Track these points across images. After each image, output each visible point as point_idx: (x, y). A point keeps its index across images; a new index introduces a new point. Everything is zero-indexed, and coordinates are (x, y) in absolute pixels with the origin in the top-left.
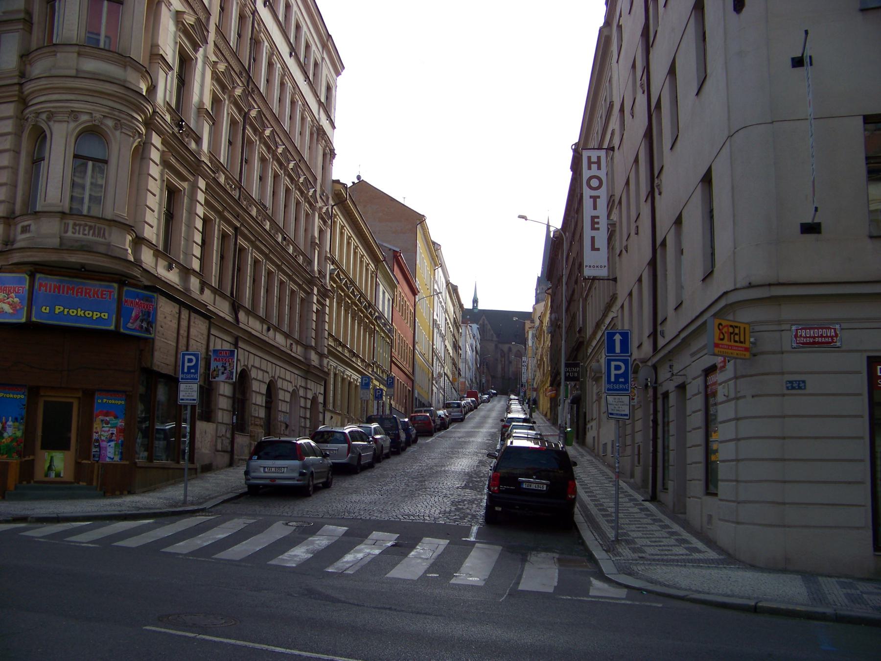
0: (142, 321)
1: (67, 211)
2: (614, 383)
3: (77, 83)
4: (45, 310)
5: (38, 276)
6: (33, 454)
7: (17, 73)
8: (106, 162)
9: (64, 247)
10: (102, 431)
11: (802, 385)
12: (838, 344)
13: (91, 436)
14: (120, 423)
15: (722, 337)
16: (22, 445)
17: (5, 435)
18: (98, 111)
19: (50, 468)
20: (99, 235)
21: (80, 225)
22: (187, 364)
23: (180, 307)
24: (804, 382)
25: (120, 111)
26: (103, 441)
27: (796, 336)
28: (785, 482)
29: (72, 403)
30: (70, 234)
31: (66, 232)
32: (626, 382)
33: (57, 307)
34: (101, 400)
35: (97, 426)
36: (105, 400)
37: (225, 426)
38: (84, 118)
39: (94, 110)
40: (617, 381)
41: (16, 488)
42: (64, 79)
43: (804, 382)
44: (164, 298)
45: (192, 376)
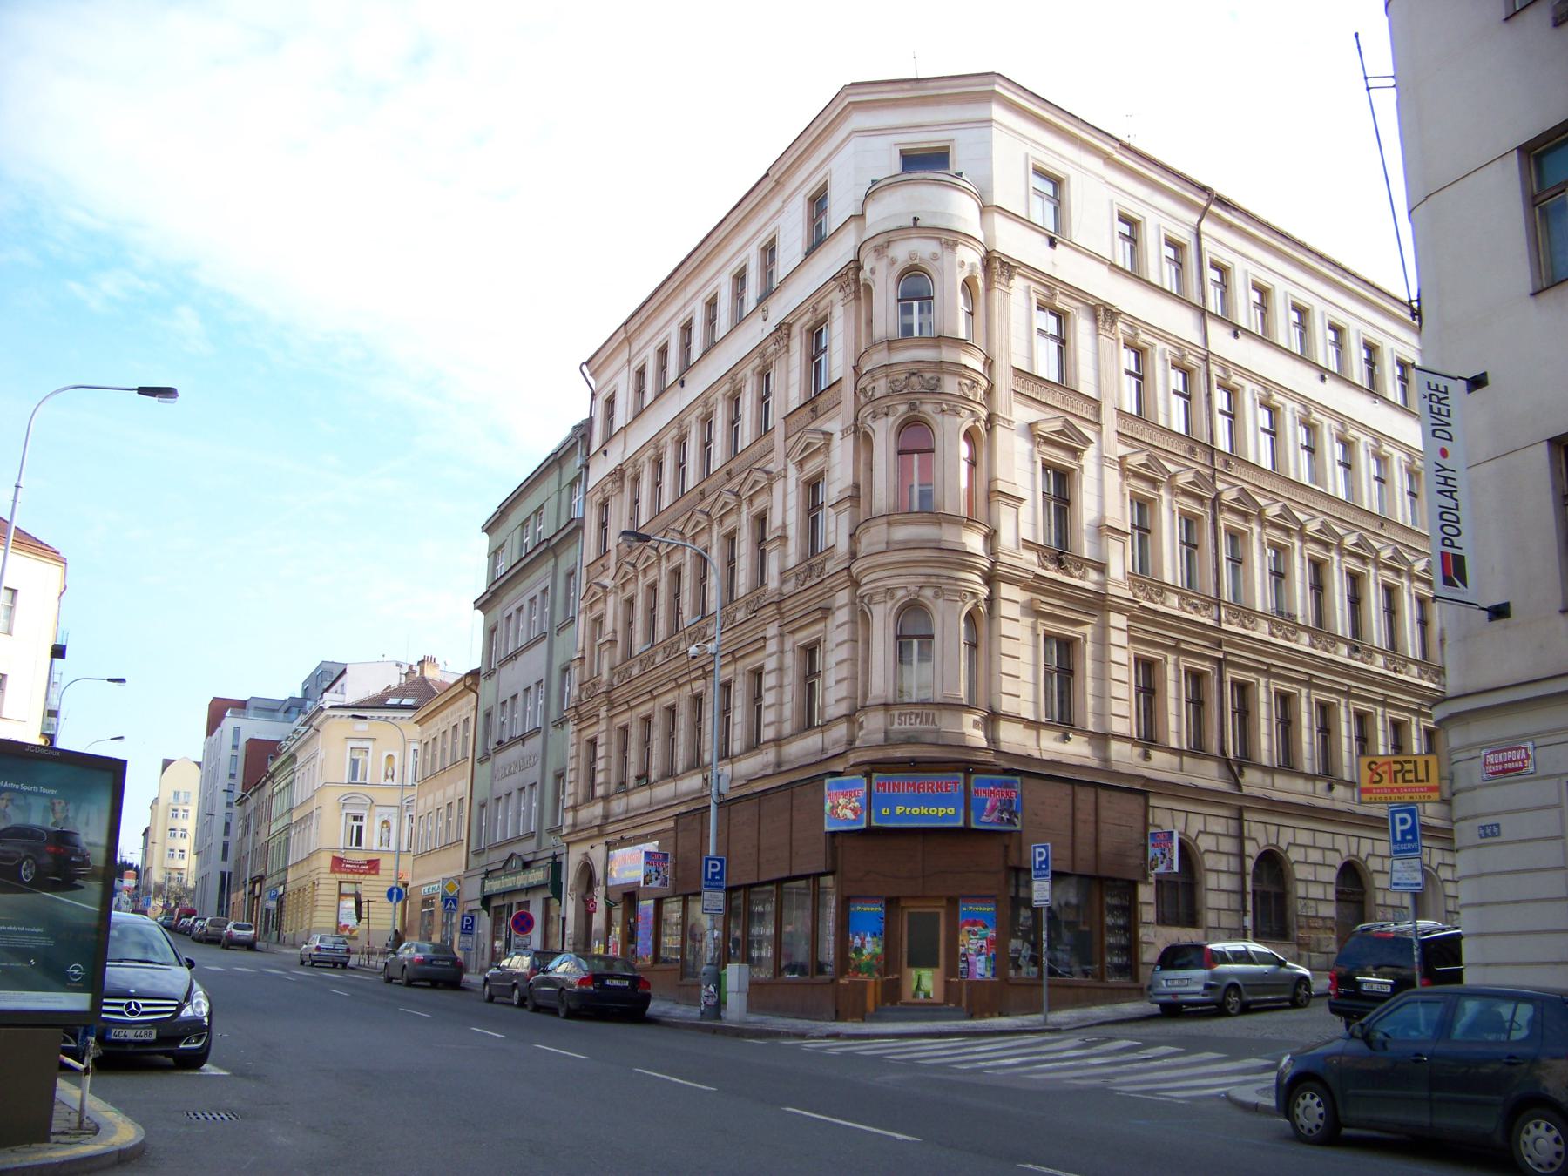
0: (1001, 812)
1: (891, 701)
2: (1401, 842)
3: (888, 558)
5: (875, 775)
6: (900, 972)
7: (848, 556)
8: (932, 637)
9: (889, 741)
10: (969, 943)
11: (1495, 830)
12: (1531, 769)
13: (958, 950)
14: (991, 933)
15: (1377, 778)
16: (883, 962)
17: (865, 952)
18: (913, 583)
19: (918, 988)
20: (927, 722)
21: (906, 714)
22: (1399, 828)
23: (1073, 788)
24: (1498, 826)
25: (938, 576)
26: (971, 955)
27: (1485, 765)
28: (1487, 965)
29: (938, 914)
30: (896, 726)
31: (892, 724)
32: (1415, 839)
33: (898, 807)
34: (967, 908)
35: (963, 938)
36: (970, 908)
37: (1227, 931)
38: (900, 593)
39: (908, 583)
40: (1404, 840)
41: (876, 1010)
42: (875, 556)
43: (1498, 826)
45: (717, 883)
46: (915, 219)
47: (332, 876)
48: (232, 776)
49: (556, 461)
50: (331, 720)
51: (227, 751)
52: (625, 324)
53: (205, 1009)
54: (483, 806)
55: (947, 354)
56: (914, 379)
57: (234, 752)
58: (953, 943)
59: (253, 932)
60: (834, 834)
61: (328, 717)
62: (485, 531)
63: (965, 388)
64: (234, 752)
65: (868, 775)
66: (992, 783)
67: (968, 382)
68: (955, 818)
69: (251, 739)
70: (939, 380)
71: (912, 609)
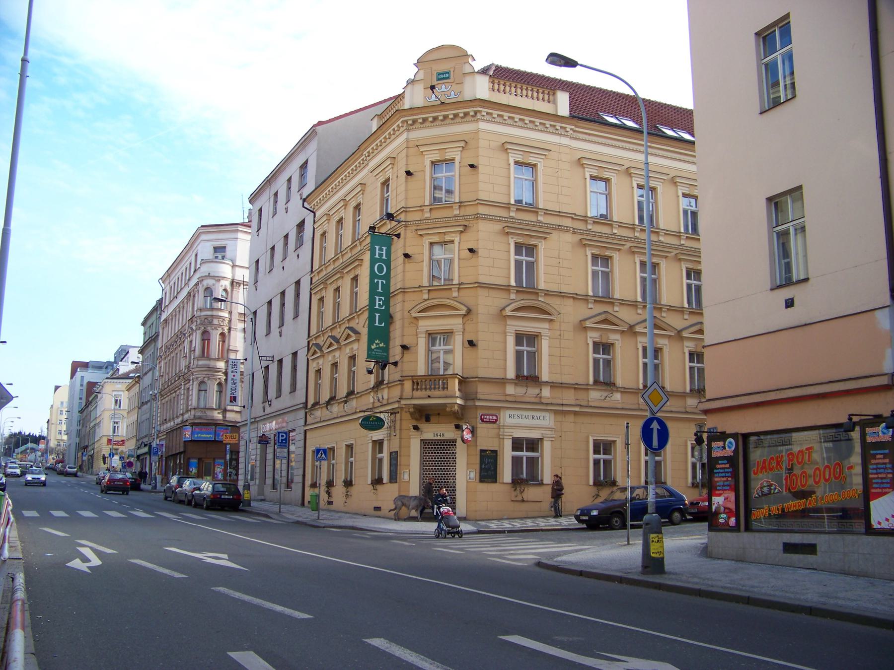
1: (196, 407)
4: (196, 436)
14: (223, 467)
22: (280, 438)
25: (208, 374)
34: (217, 461)
35: (216, 469)
44: (861, 468)
46: (209, 274)
47: (107, 446)
48: (81, 399)
49: (155, 309)
50: (106, 383)
51: (78, 387)
52: (168, 271)
53: (4, 481)
54: (140, 424)
55: (215, 313)
56: (206, 320)
57: (81, 388)
58: (214, 470)
59: (76, 469)
60: (185, 441)
61: (105, 382)
62: (142, 325)
63: (220, 322)
64: (81, 388)
65: (191, 426)
66: (222, 428)
67: (221, 320)
68: (212, 437)
69: (88, 382)
70: (212, 320)
71: (202, 383)
